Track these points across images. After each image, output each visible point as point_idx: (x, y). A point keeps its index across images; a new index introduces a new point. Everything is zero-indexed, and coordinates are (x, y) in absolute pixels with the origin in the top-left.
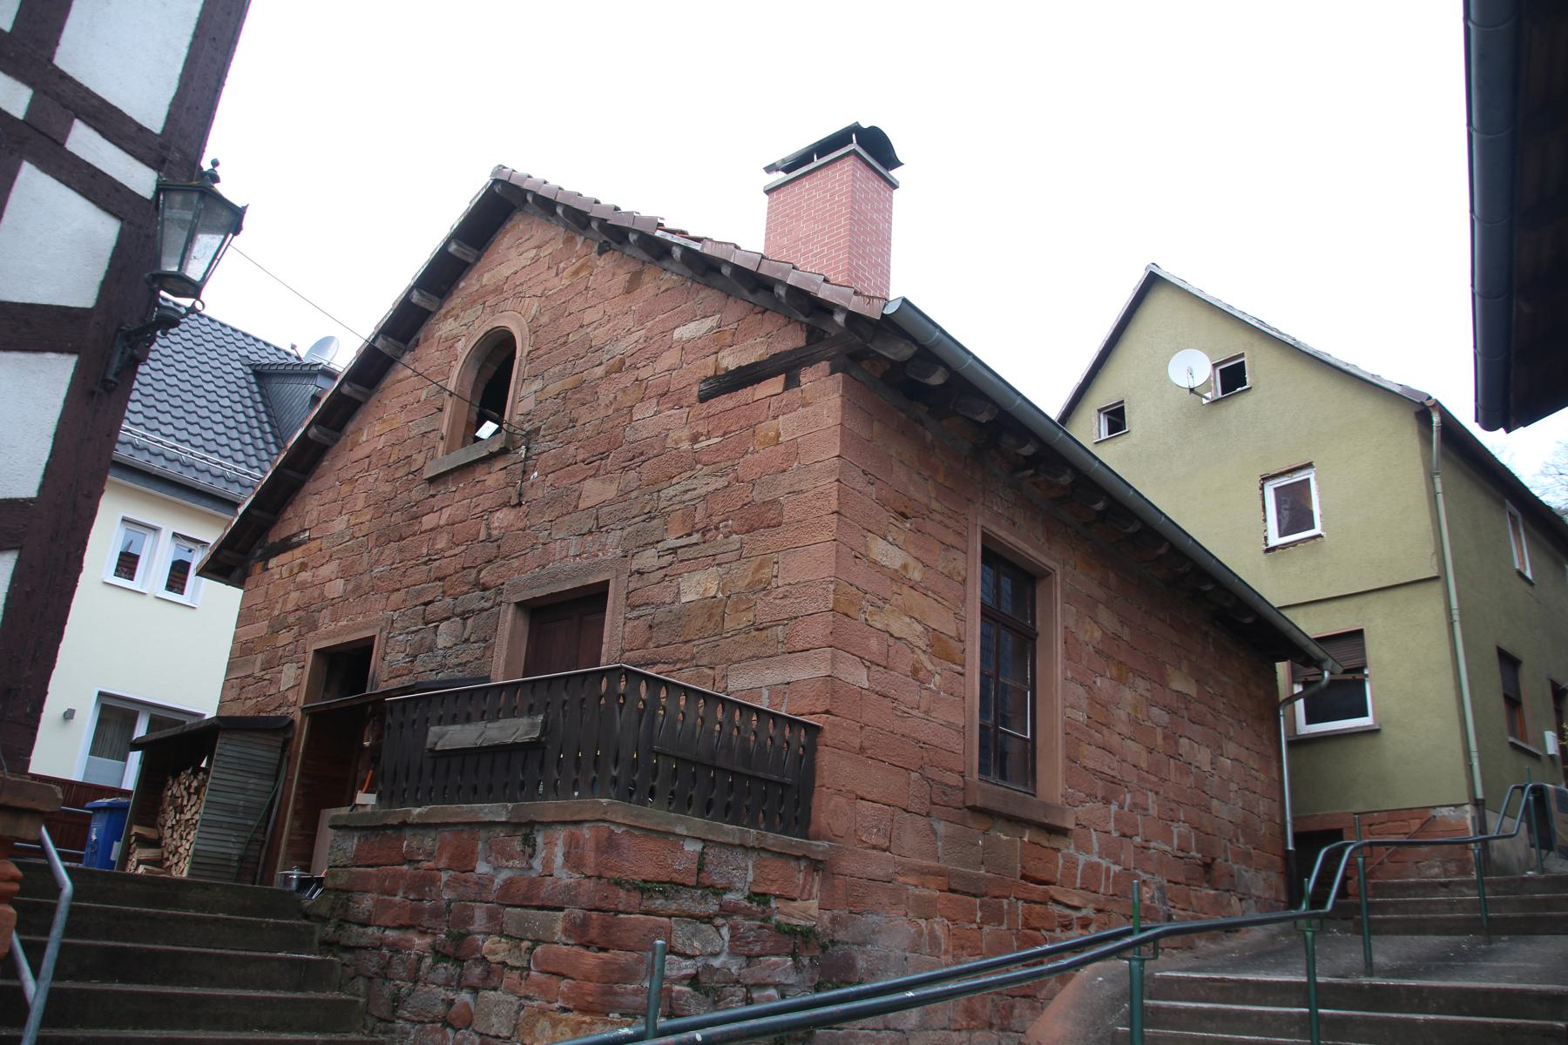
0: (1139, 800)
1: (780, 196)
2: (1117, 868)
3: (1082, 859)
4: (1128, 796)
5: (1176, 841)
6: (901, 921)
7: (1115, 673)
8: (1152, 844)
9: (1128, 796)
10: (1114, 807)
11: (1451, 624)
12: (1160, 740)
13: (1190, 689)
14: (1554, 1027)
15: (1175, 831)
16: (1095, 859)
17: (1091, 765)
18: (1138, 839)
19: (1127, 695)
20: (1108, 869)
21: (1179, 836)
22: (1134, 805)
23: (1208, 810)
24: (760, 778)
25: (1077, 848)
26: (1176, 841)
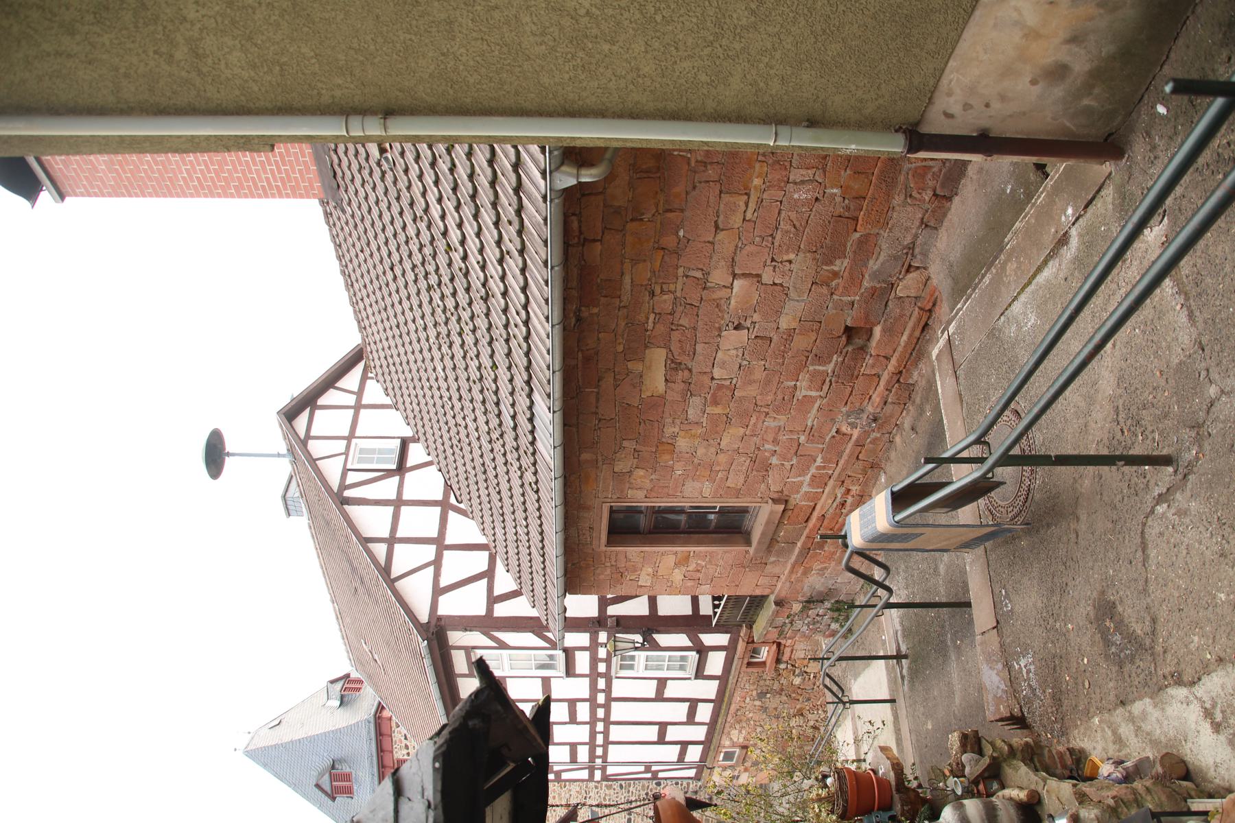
0: (770, 437)
1: (66, 188)
2: (819, 460)
3: (805, 488)
4: (767, 446)
5: (814, 394)
6: (811, 579)
7: (666, 457)
8: (809, 424)
9: (767, 446)
10: (774, 461)
11: (245, 144)
12: (718, 410)
13: (658, 357)
14: (857, 143)
15: (804, 393)
16: (808, 478)
17: (742, 481)
18: (803, 439)
19: (682, 444)
20: (818, 468)
21: (810, 388)
22: (775, 441)
23: (791, 333)
24: (846, 546)
25: (798, 492)
26: (814, 394)
